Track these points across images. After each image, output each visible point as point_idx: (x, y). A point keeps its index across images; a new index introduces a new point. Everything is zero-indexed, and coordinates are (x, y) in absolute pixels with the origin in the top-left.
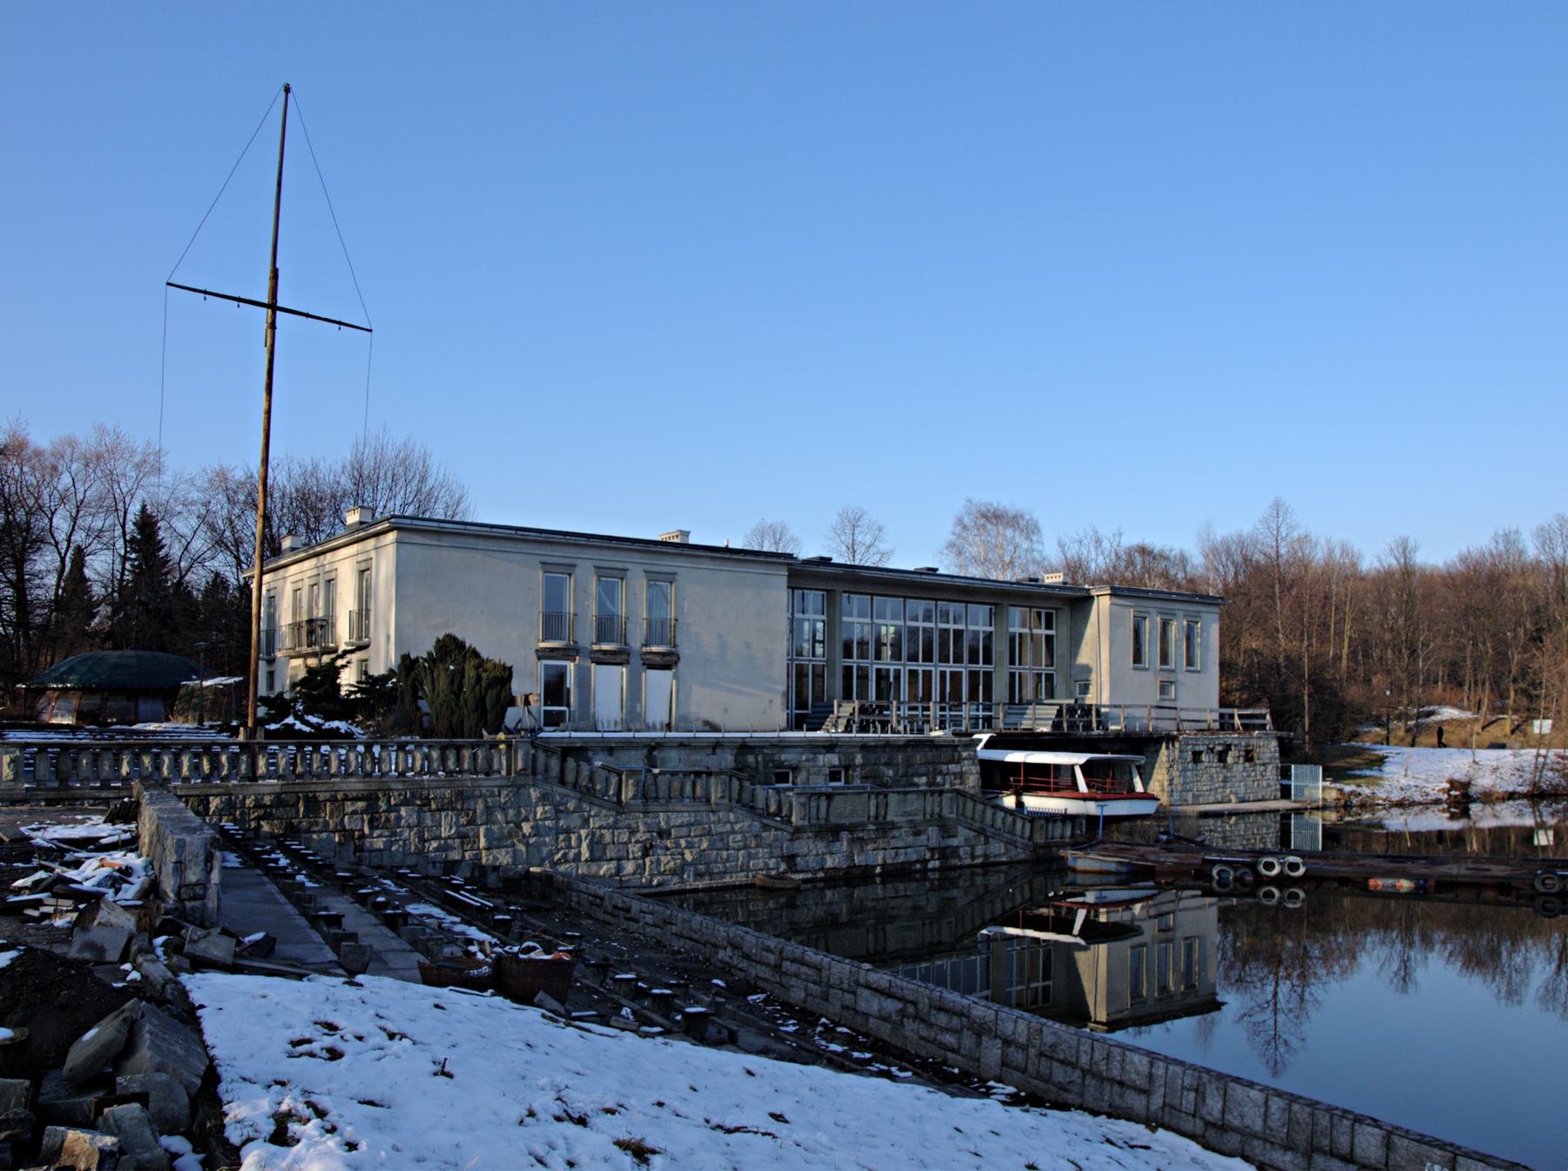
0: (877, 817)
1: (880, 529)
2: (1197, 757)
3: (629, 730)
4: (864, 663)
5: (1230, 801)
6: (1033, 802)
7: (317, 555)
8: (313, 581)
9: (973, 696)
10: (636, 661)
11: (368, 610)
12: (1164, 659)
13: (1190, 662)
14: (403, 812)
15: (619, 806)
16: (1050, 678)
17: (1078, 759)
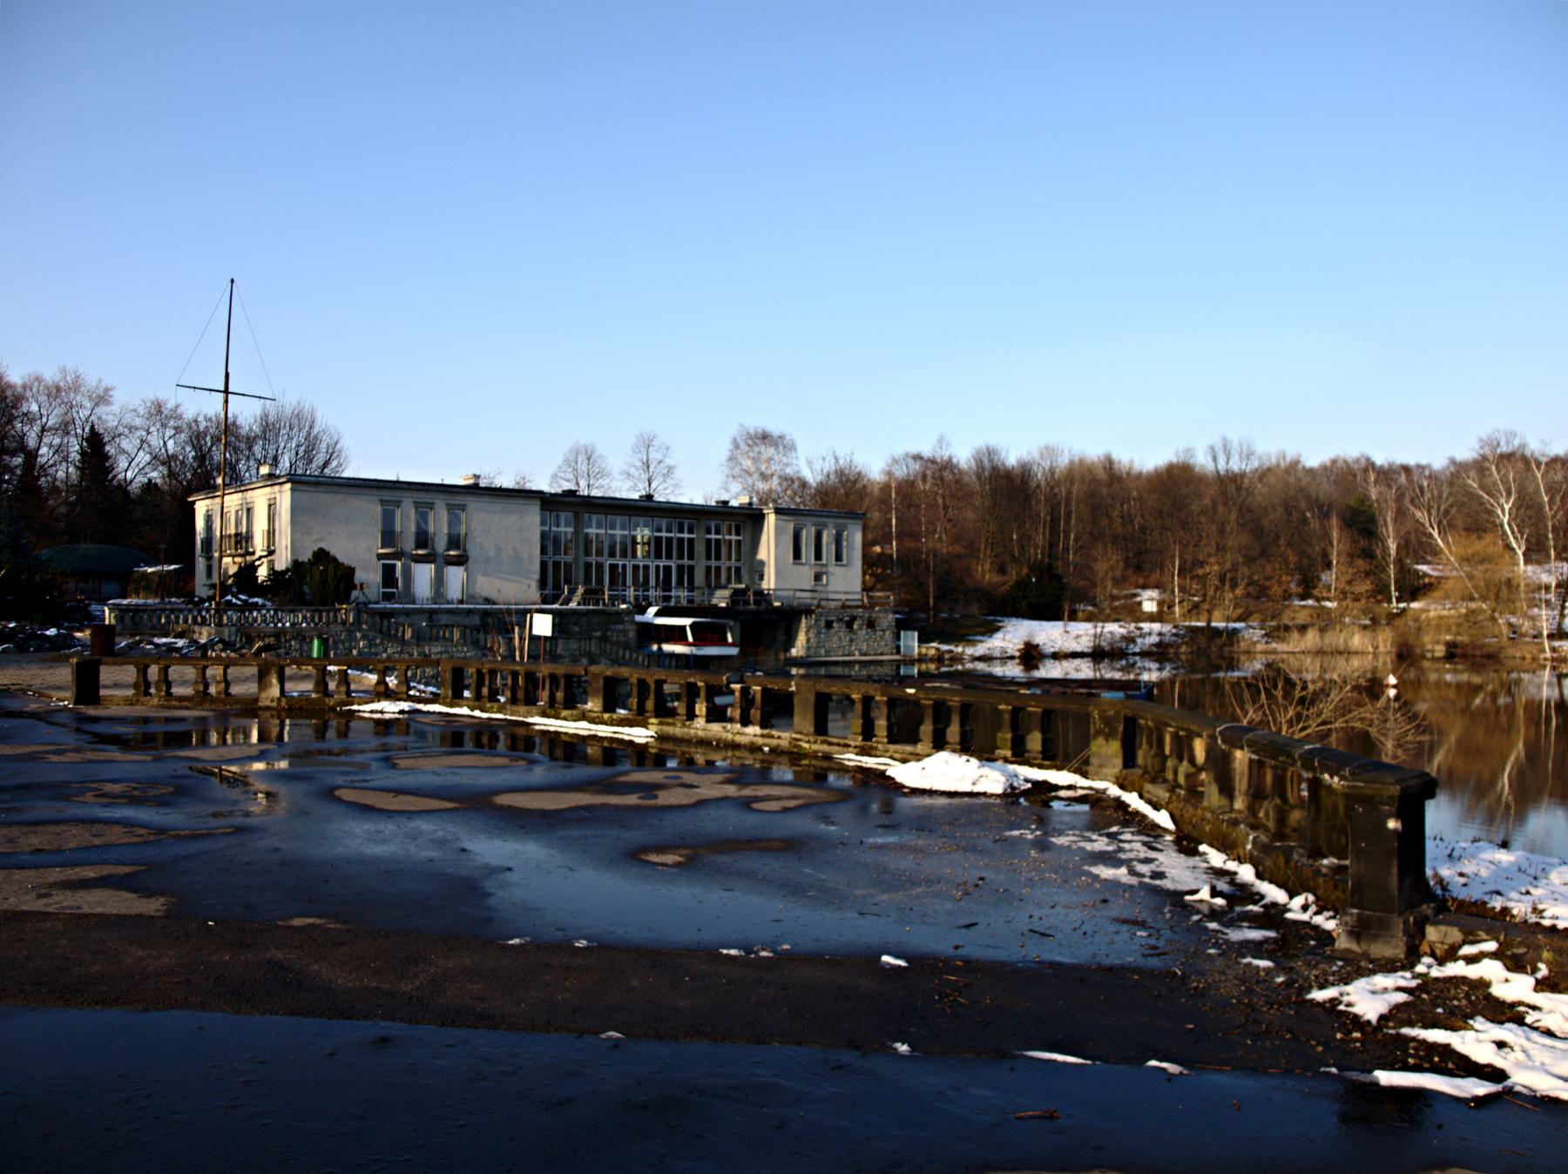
0: (551, 650)
1: (668, 449)
2: (829, 625)
3: (436, 604)
4: (600, 559)
5: (854, 655)
6: (667, 648)
7: (242, 491)
8: (238, 508)
9: (680, 583)
10: (440, 560)
11: (274, 530)
12: (818, 556)
13: (839, 558)
14: (293, 643)
15: (403, 642)
16: (738, 570)
17: (686, 622)
